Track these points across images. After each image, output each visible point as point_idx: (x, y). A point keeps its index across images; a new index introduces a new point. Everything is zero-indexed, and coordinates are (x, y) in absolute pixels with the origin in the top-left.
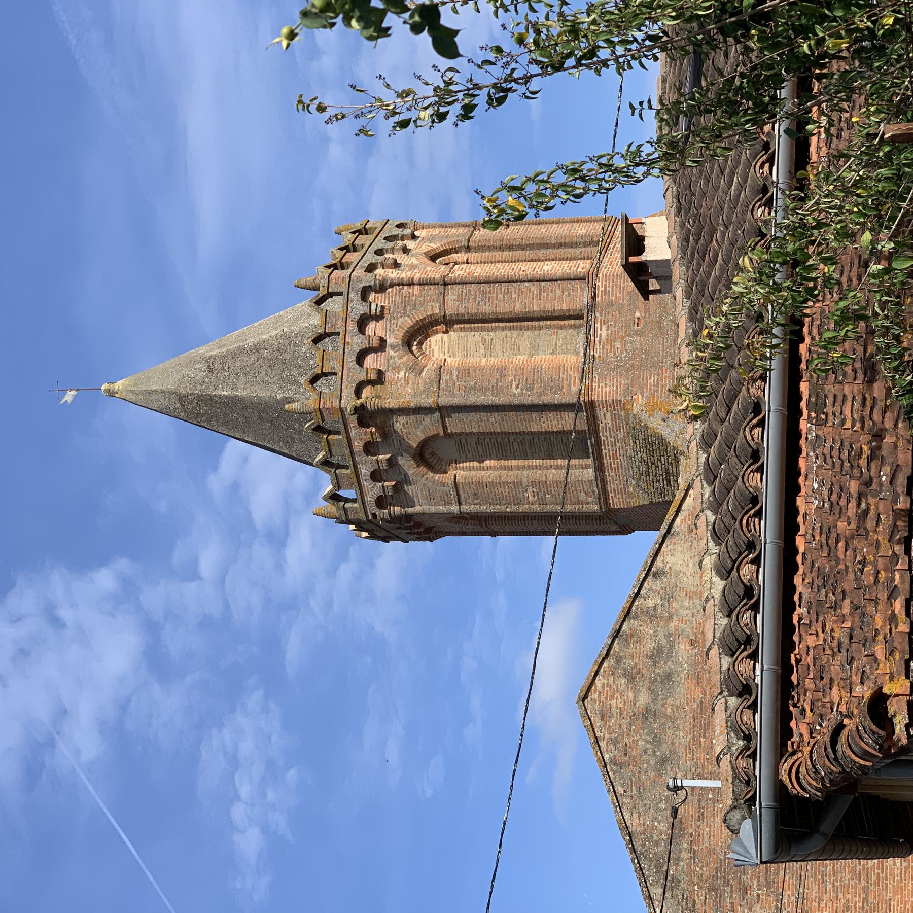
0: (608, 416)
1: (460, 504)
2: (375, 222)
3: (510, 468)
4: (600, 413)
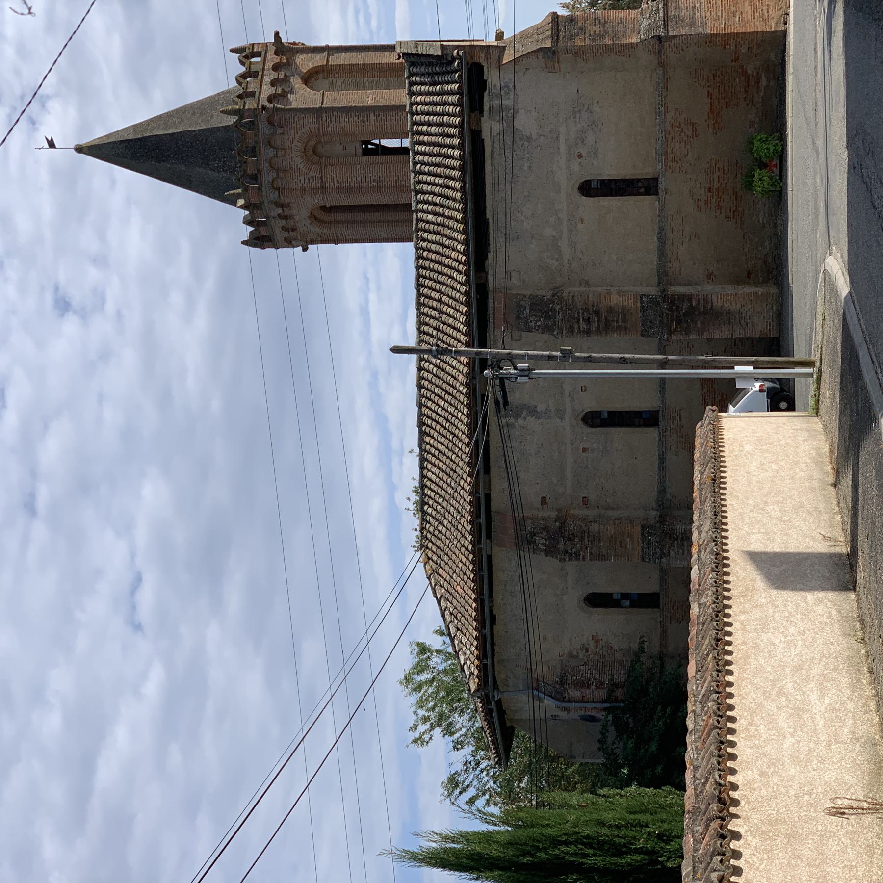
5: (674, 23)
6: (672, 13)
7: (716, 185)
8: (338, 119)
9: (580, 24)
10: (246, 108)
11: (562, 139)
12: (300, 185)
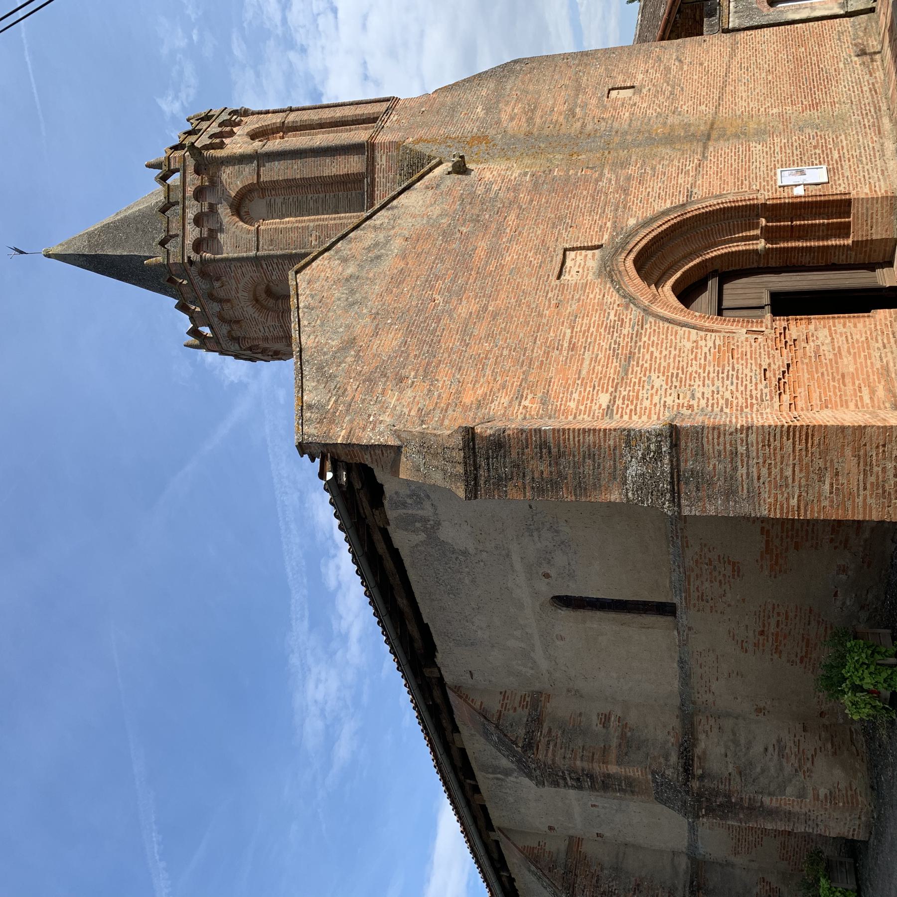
0: (384, 157)
1: (258, 250)
2: (216, 111)
3: (302, 222)
4: (378, 155)
5: (692, 487)
6: (688, 465)
7: (773, 629)
8: (280, 267)
9: (514, 455)
10: (171, 261)
11: (515, 558)
12: (261, 334)
